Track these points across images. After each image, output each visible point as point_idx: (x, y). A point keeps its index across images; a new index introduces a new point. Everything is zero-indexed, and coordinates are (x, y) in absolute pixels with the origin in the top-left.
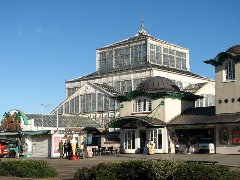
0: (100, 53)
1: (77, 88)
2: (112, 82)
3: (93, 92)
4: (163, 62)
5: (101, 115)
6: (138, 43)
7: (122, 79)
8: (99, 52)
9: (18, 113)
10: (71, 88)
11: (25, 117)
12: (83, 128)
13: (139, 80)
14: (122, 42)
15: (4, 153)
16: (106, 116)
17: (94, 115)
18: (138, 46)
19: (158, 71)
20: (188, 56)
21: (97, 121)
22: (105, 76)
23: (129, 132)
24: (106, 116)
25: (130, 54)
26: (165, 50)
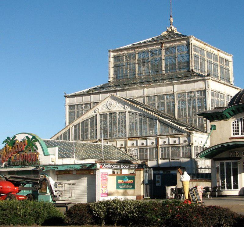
0: (115, 57)
1: (77, 105)
2: (143, 97)
3: (120, 109)
4: (206, 71)
5: (135, 142)
6: (175, 43)
7: (158, 92)
8: (112, 54)
9: (32, 138)
10: (74, 105)
11: (44, 145)
12: (115, 161)
13: (76, 106)
14: (143, 43)
15: (20, 198)
16: (143, 144)
17: (123, 143)
18: (176, 47)
19: (214, 82)
20: (231, 64)
21: (128, 151)
22: (131, 88)
23: (228, 164)
24: (143, 144)
25: (163, 58)
26: (209, 54)
